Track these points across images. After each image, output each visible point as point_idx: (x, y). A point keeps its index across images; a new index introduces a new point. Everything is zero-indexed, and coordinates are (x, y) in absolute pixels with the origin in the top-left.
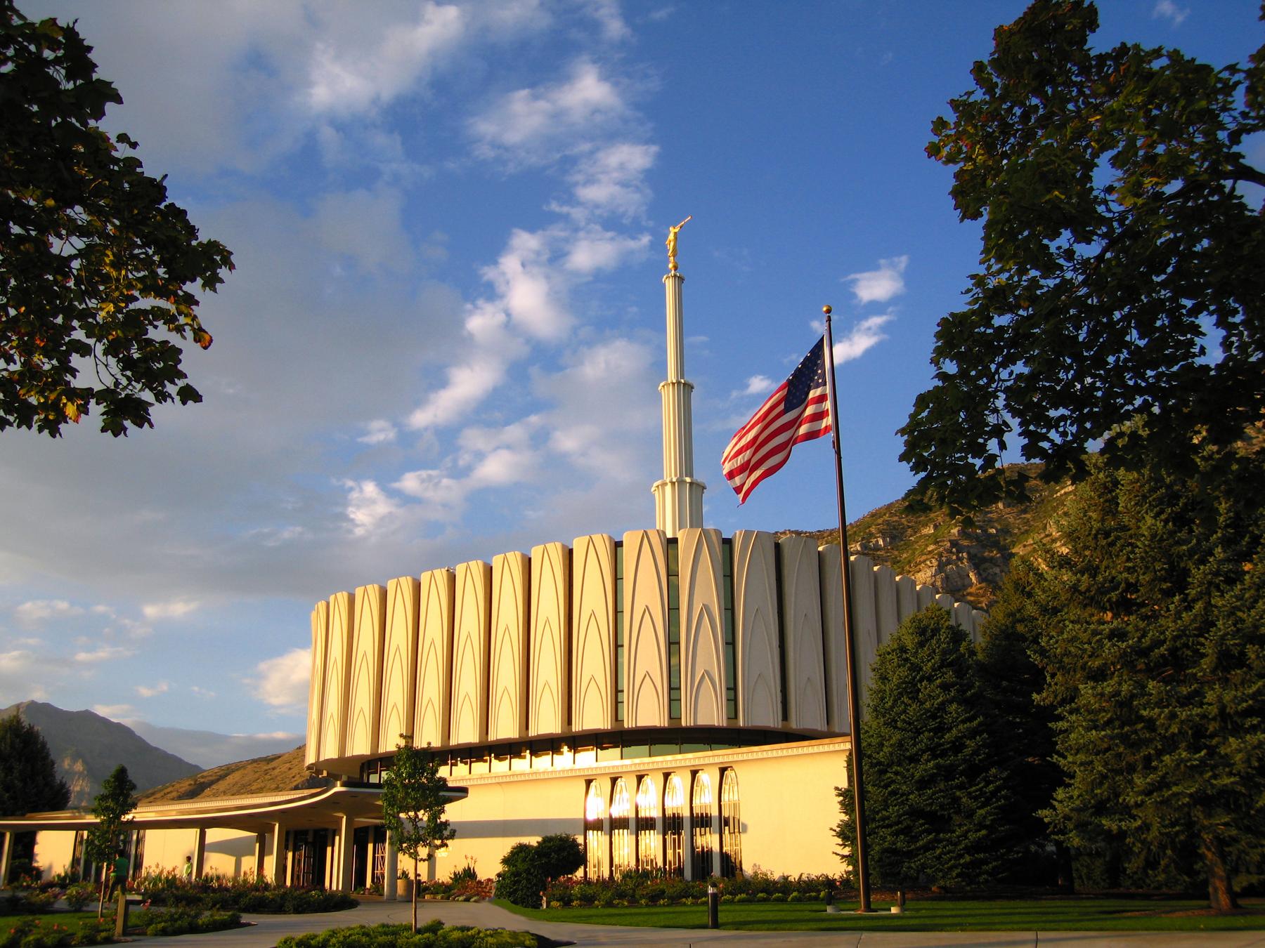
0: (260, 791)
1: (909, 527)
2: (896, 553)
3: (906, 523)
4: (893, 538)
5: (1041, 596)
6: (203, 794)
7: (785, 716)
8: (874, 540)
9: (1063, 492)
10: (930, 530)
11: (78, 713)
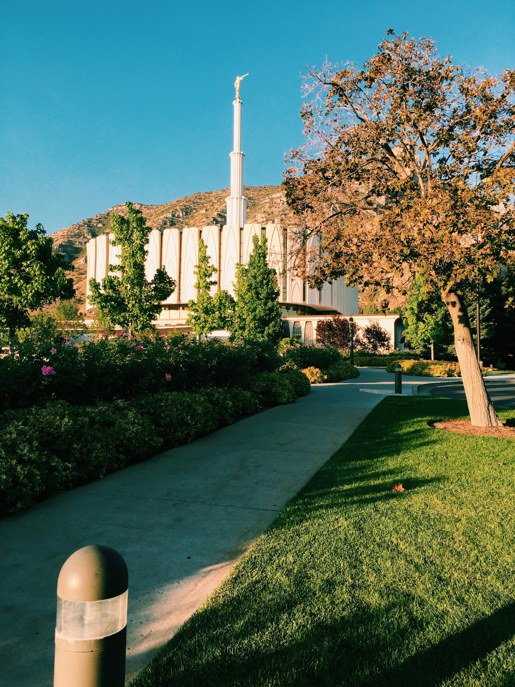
0: (434, 355)
1: (194, 209)
2: (188, 220)
3: (193, 207)
4: (186, 213)
5: (370, 238)
6: (385, 397)
7: (304, 300)
8: (178, 213)
9: (264, 202)
10: (203, 211)
11: (60, 570)
